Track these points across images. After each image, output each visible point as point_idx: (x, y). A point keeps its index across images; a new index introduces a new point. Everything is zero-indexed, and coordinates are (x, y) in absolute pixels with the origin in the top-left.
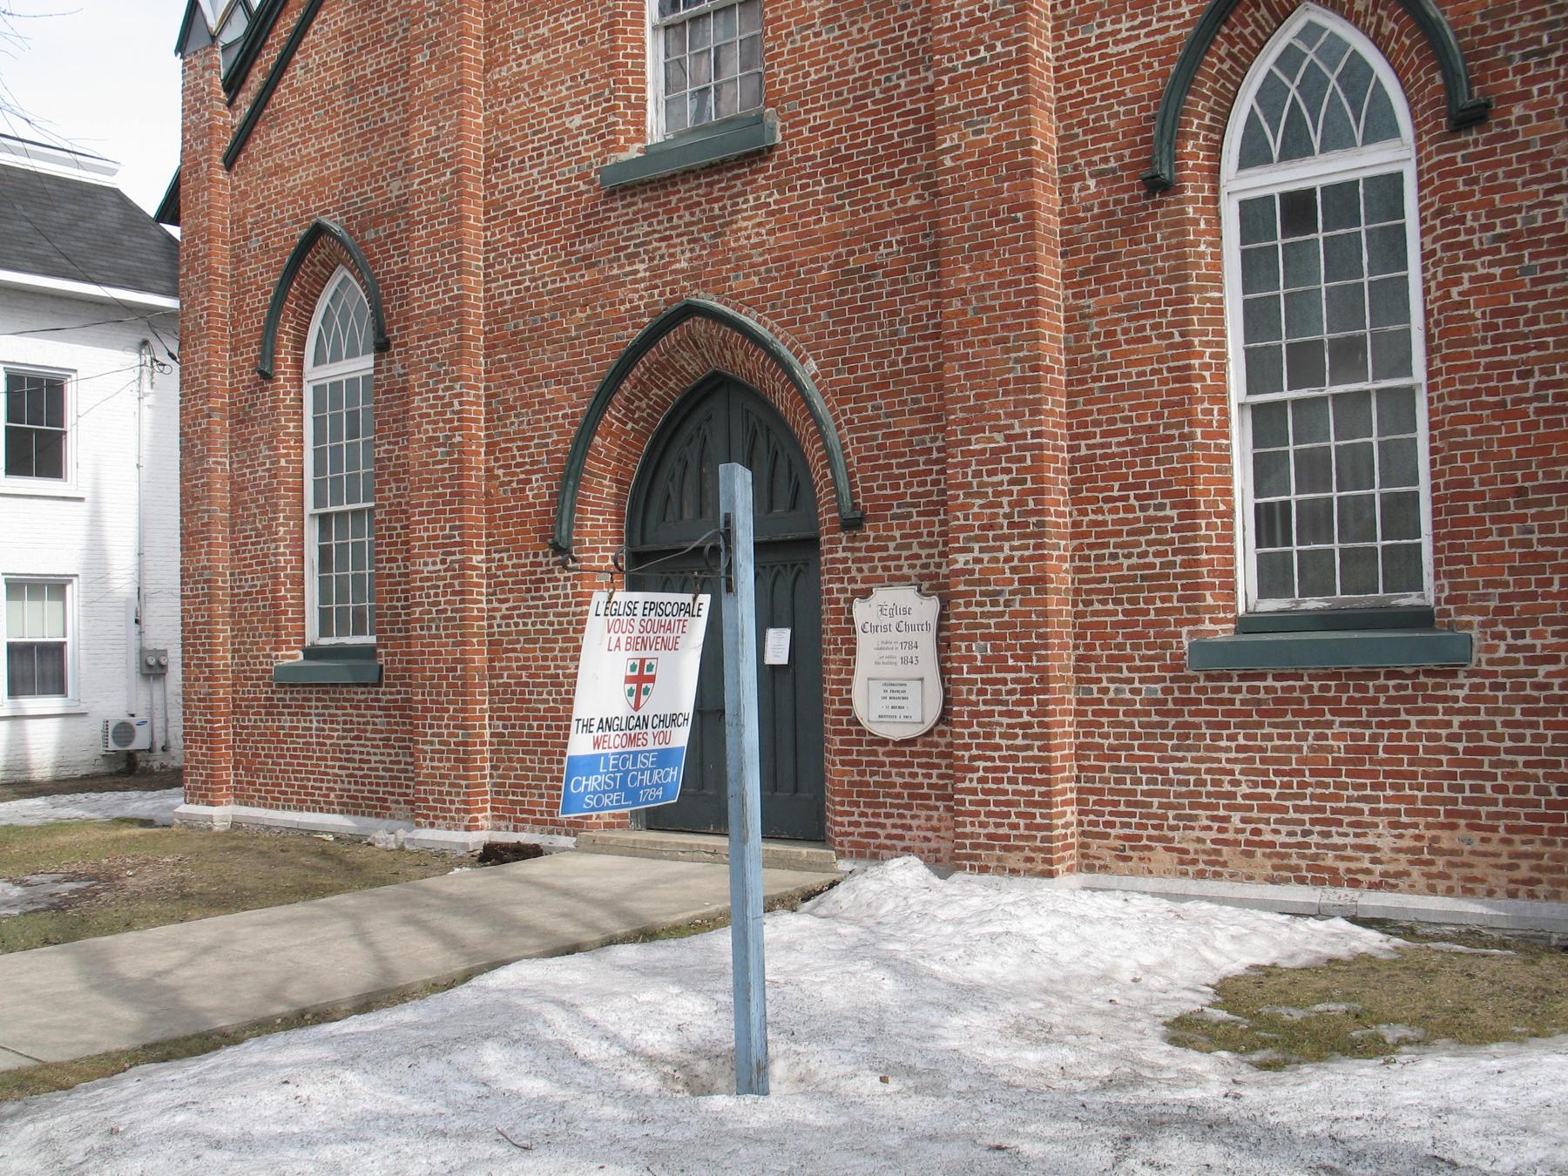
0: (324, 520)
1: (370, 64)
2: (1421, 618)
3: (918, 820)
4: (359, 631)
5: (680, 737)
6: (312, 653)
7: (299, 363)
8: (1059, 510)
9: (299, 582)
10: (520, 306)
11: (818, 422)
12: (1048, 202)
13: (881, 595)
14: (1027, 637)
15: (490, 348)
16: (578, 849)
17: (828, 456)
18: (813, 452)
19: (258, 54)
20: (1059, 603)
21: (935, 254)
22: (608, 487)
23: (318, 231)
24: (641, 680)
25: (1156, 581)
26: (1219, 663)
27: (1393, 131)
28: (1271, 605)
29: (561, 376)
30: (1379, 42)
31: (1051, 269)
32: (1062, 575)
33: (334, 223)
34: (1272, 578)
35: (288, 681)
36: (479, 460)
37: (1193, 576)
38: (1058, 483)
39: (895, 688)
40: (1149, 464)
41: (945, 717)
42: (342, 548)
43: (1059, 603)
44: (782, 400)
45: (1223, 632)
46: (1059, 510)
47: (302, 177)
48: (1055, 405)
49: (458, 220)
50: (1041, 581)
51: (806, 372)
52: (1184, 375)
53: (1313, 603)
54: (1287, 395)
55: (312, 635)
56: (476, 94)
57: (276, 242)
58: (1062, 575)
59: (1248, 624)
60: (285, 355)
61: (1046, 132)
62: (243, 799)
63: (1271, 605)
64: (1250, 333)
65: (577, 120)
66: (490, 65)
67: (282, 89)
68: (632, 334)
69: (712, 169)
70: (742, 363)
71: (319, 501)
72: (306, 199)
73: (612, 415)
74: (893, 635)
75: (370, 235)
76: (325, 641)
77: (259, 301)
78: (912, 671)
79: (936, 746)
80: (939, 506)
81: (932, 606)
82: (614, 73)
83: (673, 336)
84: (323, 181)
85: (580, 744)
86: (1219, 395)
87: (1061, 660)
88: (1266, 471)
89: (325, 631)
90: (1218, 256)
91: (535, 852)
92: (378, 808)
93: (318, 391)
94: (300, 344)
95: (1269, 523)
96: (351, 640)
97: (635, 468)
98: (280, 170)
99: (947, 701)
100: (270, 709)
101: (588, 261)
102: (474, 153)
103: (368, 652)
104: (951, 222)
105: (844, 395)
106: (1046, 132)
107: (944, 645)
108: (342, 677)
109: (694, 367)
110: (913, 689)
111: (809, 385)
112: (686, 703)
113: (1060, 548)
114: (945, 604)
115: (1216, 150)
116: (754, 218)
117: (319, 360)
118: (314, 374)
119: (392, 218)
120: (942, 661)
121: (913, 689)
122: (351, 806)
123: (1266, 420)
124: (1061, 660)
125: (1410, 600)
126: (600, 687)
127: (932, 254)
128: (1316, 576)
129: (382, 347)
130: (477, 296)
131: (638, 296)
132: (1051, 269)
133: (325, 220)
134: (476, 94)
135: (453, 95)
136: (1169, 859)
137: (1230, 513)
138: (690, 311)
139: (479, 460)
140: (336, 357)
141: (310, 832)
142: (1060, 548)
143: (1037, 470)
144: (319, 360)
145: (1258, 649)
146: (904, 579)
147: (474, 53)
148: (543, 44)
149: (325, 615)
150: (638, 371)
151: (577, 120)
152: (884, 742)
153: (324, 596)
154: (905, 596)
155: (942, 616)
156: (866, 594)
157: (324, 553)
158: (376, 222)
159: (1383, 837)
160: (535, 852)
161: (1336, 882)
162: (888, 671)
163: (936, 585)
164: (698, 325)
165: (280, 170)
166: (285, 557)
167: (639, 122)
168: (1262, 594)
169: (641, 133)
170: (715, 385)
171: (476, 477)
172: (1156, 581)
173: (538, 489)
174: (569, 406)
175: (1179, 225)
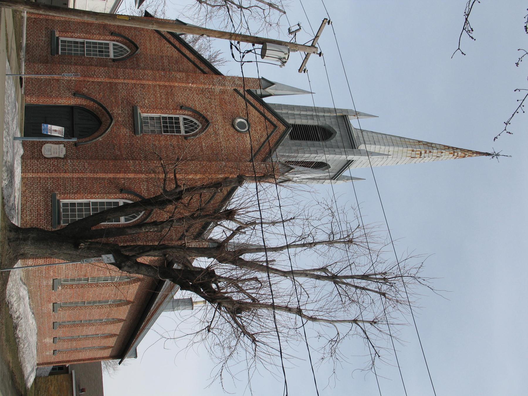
0: (83, 43)
1: (165, 61)
2: (59, 223)
3: (29, 153)
4: (62, 49)
5: (49, 134)
6: (58, 38)
7: (114, 41)
8: (76, 175)
9: (72, 37)
10: (117, 89)
11: (92, 140)
12: (121, 175)
13: (64, 149)
14: (58, 170)
15: (110, 83)
16: (22, 94)
17: (87, 141)
18: (87, 139)
19: (173, 37)
20: (62, 175)
21: (116, 159)
22: (85, 103)
23: (137, 48)
24: (56, 131)
25: (65, 189)
26: (53, 196)
27: (126, 221)
28: (61, 205)
29: (104, 96)
30: (138, 220)
31: (111, 176)
32: (66, 175)
33: (138, 51)
34: (65, 205)
35: (52, 33)
36: (91, 80)
37: (66, 194)
38: (81, 175)
39: (50, 150)
40: (83, 188)
41: (45, 158)
42: (77, 47)
43: (62, 175)
44: (96, 134)
45: (58, 198)
46: (76, 175)
47: (148, 45)
48: (91, 175)
49: (133, 79)
50: (66, 172)
51: (100, 139)
52: (94, 193)
53: (61, 210)
54: (91, 207)
55: (62, 38)
56: (155, 83)
57: (137, 38)
58: (66, 175)
59: (59, 201)
60: (115, 38)
61: (131, 176)
62: (28, 19)
63: (61, 205)
64: (100, 203)
65: (146, 102)
66: (159, 86)
67: (165, 42)
68: (109, 110)
69: (134, 124)
70: (103, 128)
71: (87, 43)
72: (144, 46)
73: (96, 105)
74: (58, 150)
75: (135, 59)
76: (60, 41)
77: (126, 33)
78: (52, 153)
79: (41, 156)
80: (78, 158)
81: (62, 156)
82: (154, 108)
83: (108, 117)
84: (146, 50)
85: (49, 126)
86: (91, 198)
87: (54, 175)
88: (80, 204)
89: (62, 41)
90: (111, 199)
91: (21, 87)
92: (27, 52)
93: (108, 44)
94: (117, 41)
95: (73, 204)
96: (60, 47)
97: (87, 108)
98: (150, 40)
99: (48, 158)
100: (47, 28)
101: (122, 102)
102: (144, 82)
103: (58, 53)
104: (119, 162)
105: (95, 144)
106: (131, 176)
107: (56, 158)
108: (53, 42)
109: (103, 120)
110: (50, 153)
111: (98, 139)
112: (53, 134)
113: (70, 175)
114: (63, 158)
115: (126, 199)
116: (125, 131)
117: (114, 45)
118: (111, 44)
119: (137, 64)
120: (54, 158)
121: (50, 153)
122: (27, 44)
123: (88, 204)
124: (54, 175)
125: (62, 222)
126: (54, 127)
127: (116, 158)
128: (65, 210)
129: (114, 60)
130: (120, 81)
131: (116, 111)
132: (111, 176)
133: (139, 49)
134: (155, 83)
135: (155, 79)
136: (24, 190)
137: (75, 199)
138: (112, 120)
139: (91, 80)
140: (114, 49)
141: (22, 36)
142: (70, 175)
143: (82, 172)
144: (114, 45)
145: (55, 203)
146: (67, 152)
147: (162, 83)
148: (161, 96)
149: (65, 42)
150: (103, 110)
151: (146, 102)
152: (41, 148)
153: (69, 42)
154: (64, 152)
155: (61, 158)
156: (65, 146)
157: (77, 43)
158: (137, 61)
159: (28, 218)
160: (21, 87)
161: (22, 212)
162: (52, 149)
163: (66, 157)
164: (109, 121)
165: (150, 40)
166: (76, 35)
167: (145, 112)
168: (63, 203)
169: (143, 112)
170: (100, 123)
171: (88, 79)
172: (65, 189)
173: (85, 90)
174: (98, 97)
175: (116, 193)
